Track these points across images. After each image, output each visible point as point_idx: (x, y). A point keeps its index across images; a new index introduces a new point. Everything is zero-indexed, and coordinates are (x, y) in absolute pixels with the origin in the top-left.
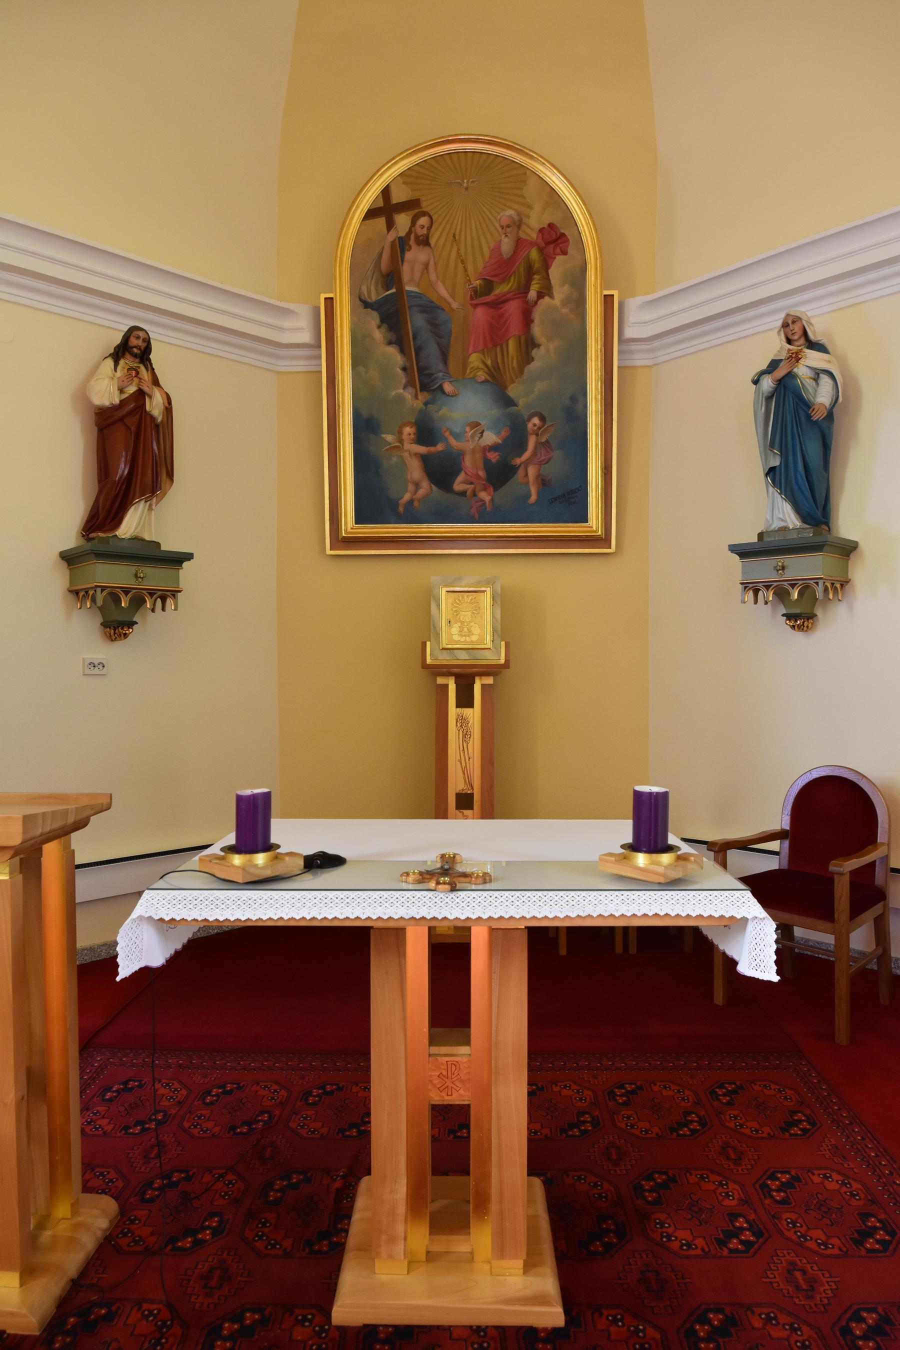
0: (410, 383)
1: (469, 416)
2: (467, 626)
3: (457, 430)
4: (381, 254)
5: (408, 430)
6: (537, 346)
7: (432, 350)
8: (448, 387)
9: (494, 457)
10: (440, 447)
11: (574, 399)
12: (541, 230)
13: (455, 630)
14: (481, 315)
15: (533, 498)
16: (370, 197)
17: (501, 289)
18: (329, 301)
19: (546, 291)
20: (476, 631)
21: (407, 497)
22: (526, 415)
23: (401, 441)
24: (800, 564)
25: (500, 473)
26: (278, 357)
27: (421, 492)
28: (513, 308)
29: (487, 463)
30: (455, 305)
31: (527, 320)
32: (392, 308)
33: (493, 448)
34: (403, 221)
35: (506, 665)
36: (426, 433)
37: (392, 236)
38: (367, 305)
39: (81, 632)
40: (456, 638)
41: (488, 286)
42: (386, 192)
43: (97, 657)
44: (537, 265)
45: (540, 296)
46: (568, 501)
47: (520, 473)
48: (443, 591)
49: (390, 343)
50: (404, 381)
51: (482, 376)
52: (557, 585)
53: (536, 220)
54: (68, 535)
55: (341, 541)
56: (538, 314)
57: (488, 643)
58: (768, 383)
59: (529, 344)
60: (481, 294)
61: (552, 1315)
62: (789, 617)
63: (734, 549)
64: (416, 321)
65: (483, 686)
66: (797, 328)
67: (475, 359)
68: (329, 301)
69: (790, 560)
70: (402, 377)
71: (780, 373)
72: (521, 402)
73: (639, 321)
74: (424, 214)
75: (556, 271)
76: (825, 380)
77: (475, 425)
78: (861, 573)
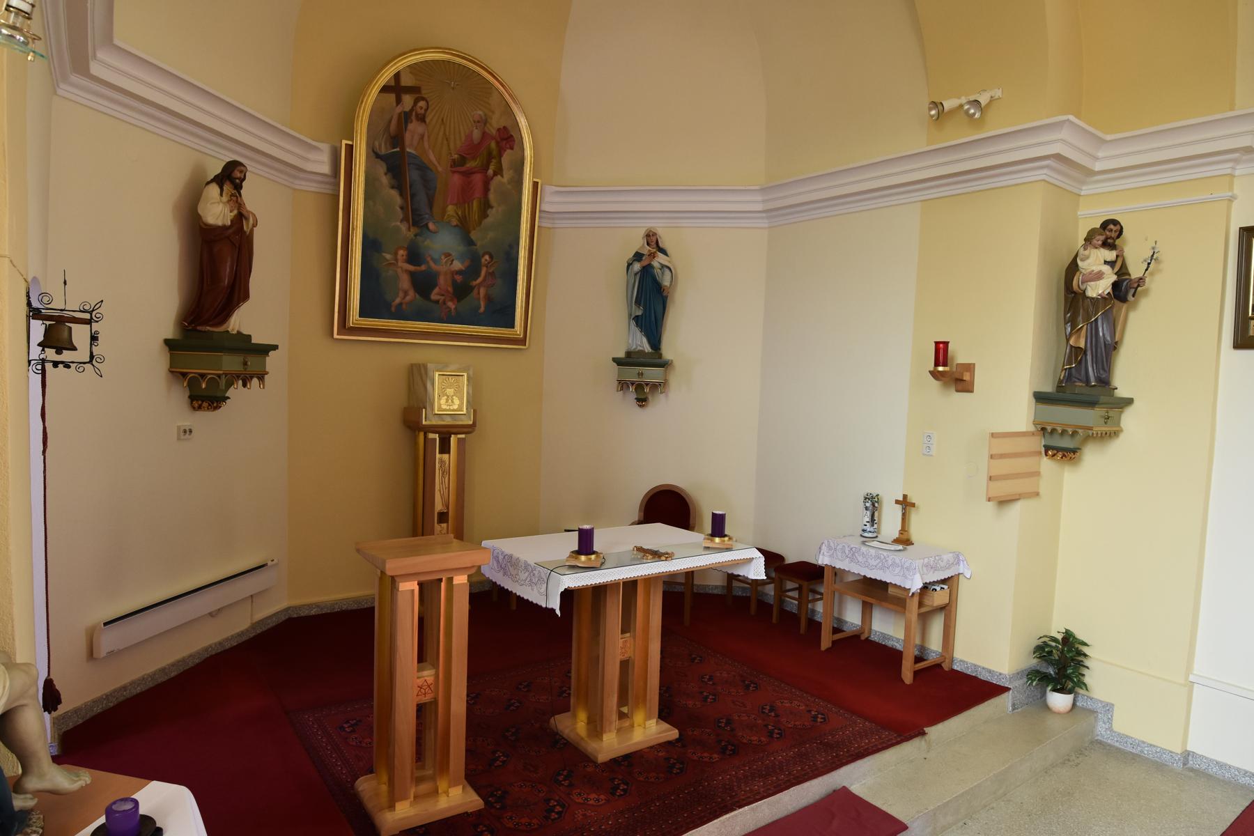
0: (405, 219)
1: (444, 247)
3: (436, 256)
4: (390, 122)
5: (401, 252)
7: (422, 198)
8: (431, 226)
9: (459, 278)
10: (423, 268)
11: (511, 246)
12: (499, 130)
13: (443, 401)
14: (456, 179)
15: (482, 309)
16: (386, 77)
17: (471, 164)
18: (350, 149)
19: (498, 171)
20: (457, 401)
21: (398, 301)
22: (481, 252)
23: (397, 260)
24: (643, 371)
25: (462, 290)
26: (295, 177)
27: (408, 298)
28: (477, 178)
29: (454, 282)
30: (440, 169)
31: (486, 190)
32: (394, 161)
33: (459, 272)
34: (408, 100)
35: (474, 425)
36: (414, 256)
37: (399, 109)
38: (378, 156)
39: (170, 403)
40: (444, 407)
42: (397, 76)
43: (186, 424)
44: (495, 153)
45: (495, 174)
46: (502, 313)
47: (475, 291)
49: (393, 187)
50: (401, 216)
51: (454, 222)
52: (497, 364)
53: (496, 123)
56: (493, 185)
58: (637, 267)
59: (486, 205)
60: (457, 164)
61: (673, 734)
63: (614, 360)
64: (413, 175)
66: (654, 239)
67: (451, 209)
70: (400, 214)
71: (645, 263)
72: (479, 243)
73: (550, 202)
74: (423, 99)
75: (507, 158)
76: (667, 272)
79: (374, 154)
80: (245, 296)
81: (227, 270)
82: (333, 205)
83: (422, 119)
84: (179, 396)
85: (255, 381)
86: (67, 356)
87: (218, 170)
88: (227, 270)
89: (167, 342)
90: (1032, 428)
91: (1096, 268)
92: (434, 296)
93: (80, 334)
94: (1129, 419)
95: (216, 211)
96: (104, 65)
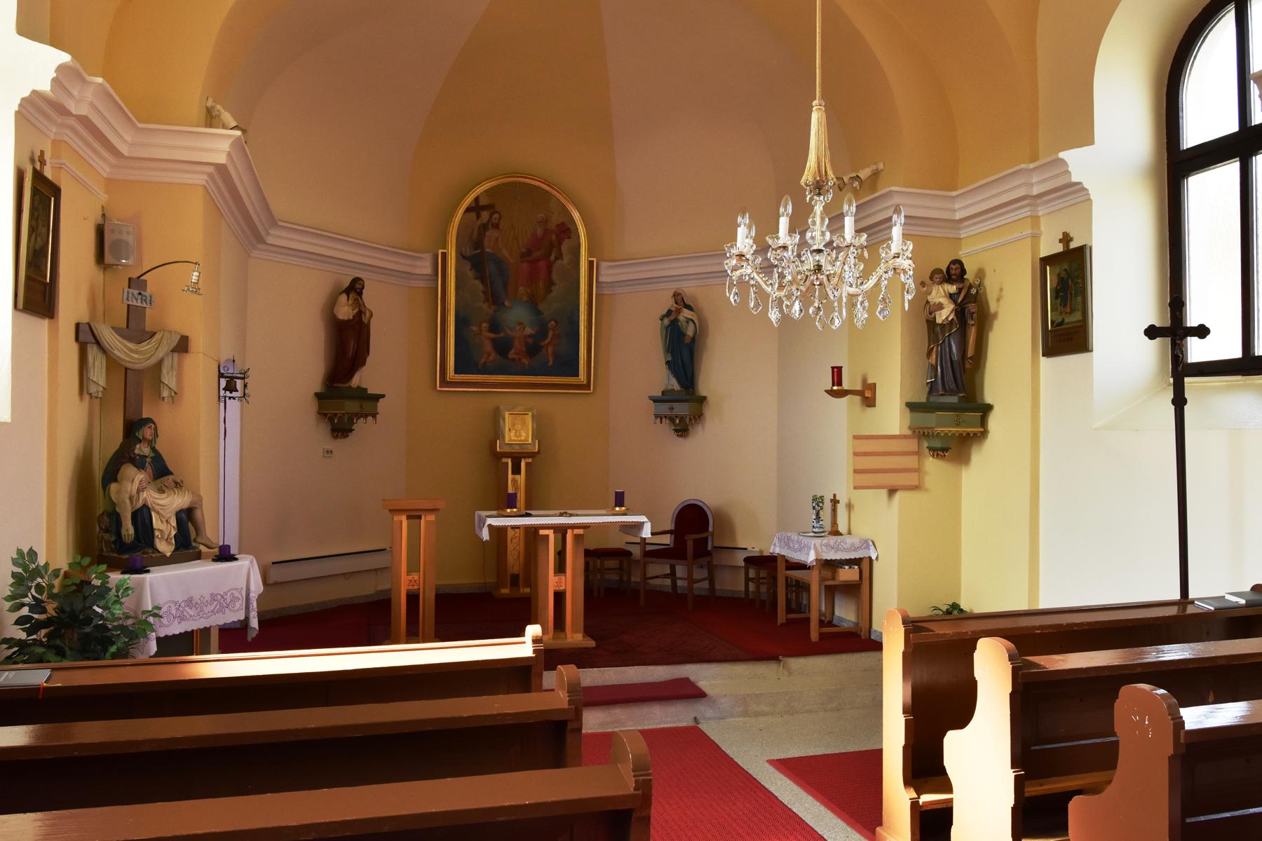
1: (517, 318)
2: (518, 432)
6: (554, 284)
8: (507, 303)
9: (530, 341)
13: (513, 433)
15: (551, 363)
16: (468, 200)
17: (536, 255)
18: (444, 255)
20: (524, 434)
21: (483, 361)
24: (683, 404)
25: (533, 349)
28: (542, 264)
31: (550, 272)
32: (477, 259)
33: (531, 336)
34: (485, 215)
36: (495, 327)
37: (479, 223)
38: (464, 257)
39: (318, 435)
41: (529, 252)
42: (477, 199)
43: (329, 447)
45: (557, 259)
46: (569, 365)
48: (507, 414)
51: (525, 299)
52: (564, 408)
53: (555, 220)
54: (317, 387)
55: (444, 382)
57: (530, 441)
58: (666, 321)
59: (550, 284)
60: (524, 256)
62: (676, 431)
65: (527, 464)
68: (444, 255)
69: (675, 405)
71: (672, 318)
73: (608, 274)
77: (520, 324)
78: (709, 413)
79: (461, 256)
80: (364, 363)
81: (352, 345)
82: (434, 295)
83: (496, 226)
84: (325, 429)
85: (370, 418)
86: (234, 394)
87: (347, 284)
88: (352, 345)
89: (316, 394)
90: (909, 432)
91: (937, 300)
92: (511, 355)
93: (239, 384)
94: (994, 422)
95: (345, 311)
96: (275, 237)
